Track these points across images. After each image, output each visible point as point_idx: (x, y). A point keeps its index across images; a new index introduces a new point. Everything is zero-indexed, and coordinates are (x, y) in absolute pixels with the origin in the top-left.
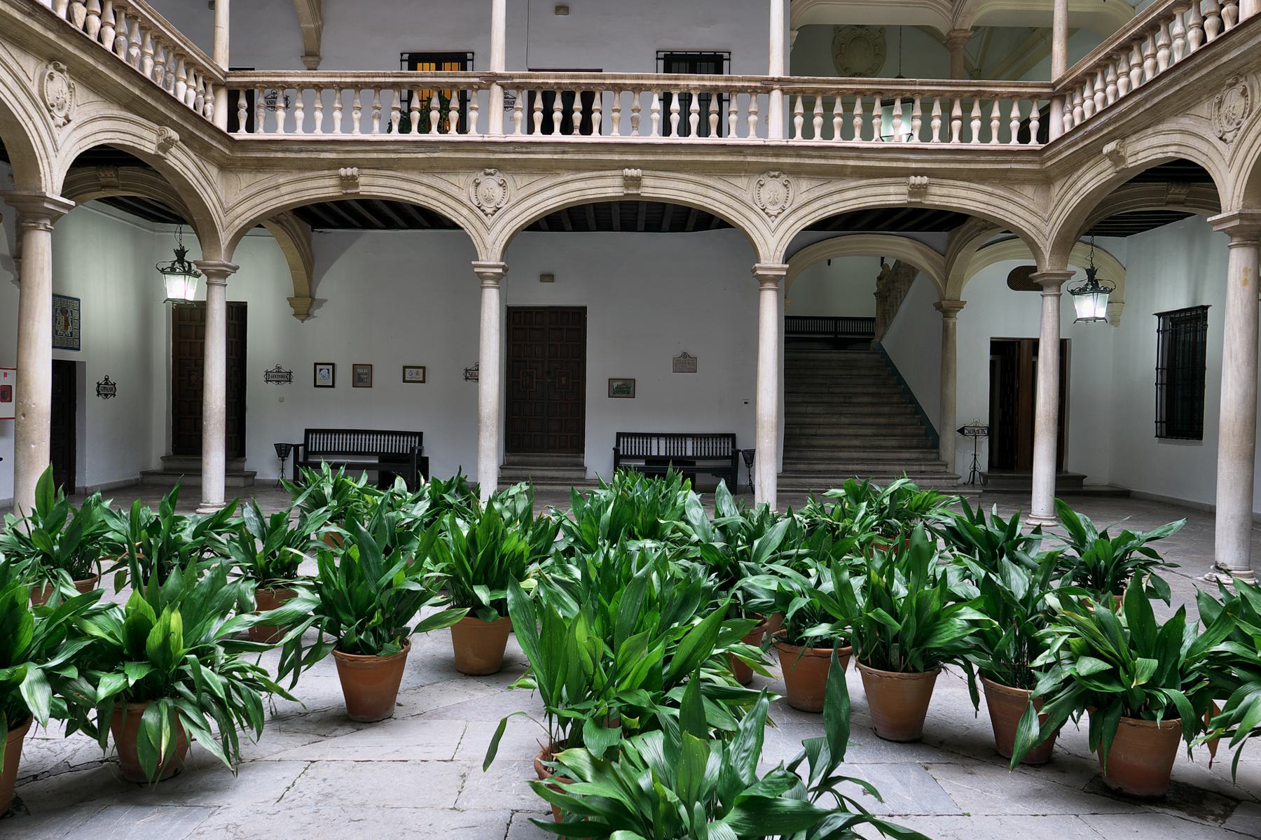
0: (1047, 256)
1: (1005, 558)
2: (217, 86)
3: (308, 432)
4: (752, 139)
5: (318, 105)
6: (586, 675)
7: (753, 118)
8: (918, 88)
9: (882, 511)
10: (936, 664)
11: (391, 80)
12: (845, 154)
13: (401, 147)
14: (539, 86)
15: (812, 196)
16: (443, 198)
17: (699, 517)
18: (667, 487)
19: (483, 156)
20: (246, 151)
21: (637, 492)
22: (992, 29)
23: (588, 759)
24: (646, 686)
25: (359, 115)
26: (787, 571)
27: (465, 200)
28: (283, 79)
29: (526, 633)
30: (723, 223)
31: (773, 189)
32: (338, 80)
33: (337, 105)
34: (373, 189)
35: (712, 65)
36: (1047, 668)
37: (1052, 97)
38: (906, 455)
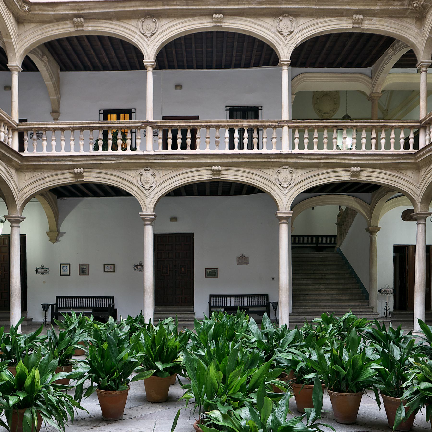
0: (419, 205)
1: (392, 343)
2: (14, 130)
3: (57, 298)
4: (274, 151)
5: (63, 138)
6: (214, 389)
7: (274, 140)
8: (354, 124)
9: (340, 328)
10: (362, 390)
11: (98, 125)
12: (319, 157)
13: (104, 158)
14: (170, 127)
15: (304, 178)
16: (125, 182)
17: (255, 329)
18: (238, 319)
19: (143, 161)
20: (29, 161)
21: (225, 320)
22: (392, 92)
23: (220, 415)
24: (240, 390)
25: (83, 142)
26: (296, 352)
27: (135, 183)
28: (45, 126)
29: (191, 372)
30: (260, 191)
31: (285, 174)
32: (72, 126)
33: (72, 138)
34: (90, 178)
35: (253, 113)
36: (408, 387)
37: (420, 127)
38: (353, 304)
